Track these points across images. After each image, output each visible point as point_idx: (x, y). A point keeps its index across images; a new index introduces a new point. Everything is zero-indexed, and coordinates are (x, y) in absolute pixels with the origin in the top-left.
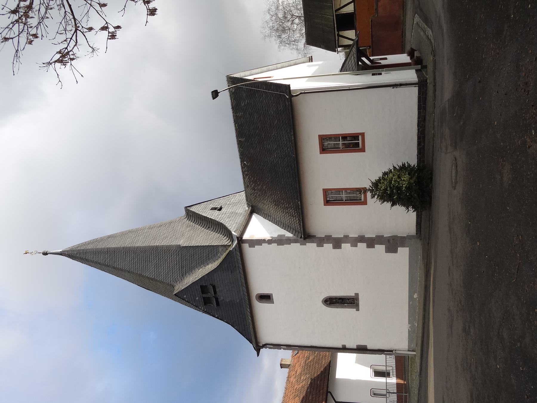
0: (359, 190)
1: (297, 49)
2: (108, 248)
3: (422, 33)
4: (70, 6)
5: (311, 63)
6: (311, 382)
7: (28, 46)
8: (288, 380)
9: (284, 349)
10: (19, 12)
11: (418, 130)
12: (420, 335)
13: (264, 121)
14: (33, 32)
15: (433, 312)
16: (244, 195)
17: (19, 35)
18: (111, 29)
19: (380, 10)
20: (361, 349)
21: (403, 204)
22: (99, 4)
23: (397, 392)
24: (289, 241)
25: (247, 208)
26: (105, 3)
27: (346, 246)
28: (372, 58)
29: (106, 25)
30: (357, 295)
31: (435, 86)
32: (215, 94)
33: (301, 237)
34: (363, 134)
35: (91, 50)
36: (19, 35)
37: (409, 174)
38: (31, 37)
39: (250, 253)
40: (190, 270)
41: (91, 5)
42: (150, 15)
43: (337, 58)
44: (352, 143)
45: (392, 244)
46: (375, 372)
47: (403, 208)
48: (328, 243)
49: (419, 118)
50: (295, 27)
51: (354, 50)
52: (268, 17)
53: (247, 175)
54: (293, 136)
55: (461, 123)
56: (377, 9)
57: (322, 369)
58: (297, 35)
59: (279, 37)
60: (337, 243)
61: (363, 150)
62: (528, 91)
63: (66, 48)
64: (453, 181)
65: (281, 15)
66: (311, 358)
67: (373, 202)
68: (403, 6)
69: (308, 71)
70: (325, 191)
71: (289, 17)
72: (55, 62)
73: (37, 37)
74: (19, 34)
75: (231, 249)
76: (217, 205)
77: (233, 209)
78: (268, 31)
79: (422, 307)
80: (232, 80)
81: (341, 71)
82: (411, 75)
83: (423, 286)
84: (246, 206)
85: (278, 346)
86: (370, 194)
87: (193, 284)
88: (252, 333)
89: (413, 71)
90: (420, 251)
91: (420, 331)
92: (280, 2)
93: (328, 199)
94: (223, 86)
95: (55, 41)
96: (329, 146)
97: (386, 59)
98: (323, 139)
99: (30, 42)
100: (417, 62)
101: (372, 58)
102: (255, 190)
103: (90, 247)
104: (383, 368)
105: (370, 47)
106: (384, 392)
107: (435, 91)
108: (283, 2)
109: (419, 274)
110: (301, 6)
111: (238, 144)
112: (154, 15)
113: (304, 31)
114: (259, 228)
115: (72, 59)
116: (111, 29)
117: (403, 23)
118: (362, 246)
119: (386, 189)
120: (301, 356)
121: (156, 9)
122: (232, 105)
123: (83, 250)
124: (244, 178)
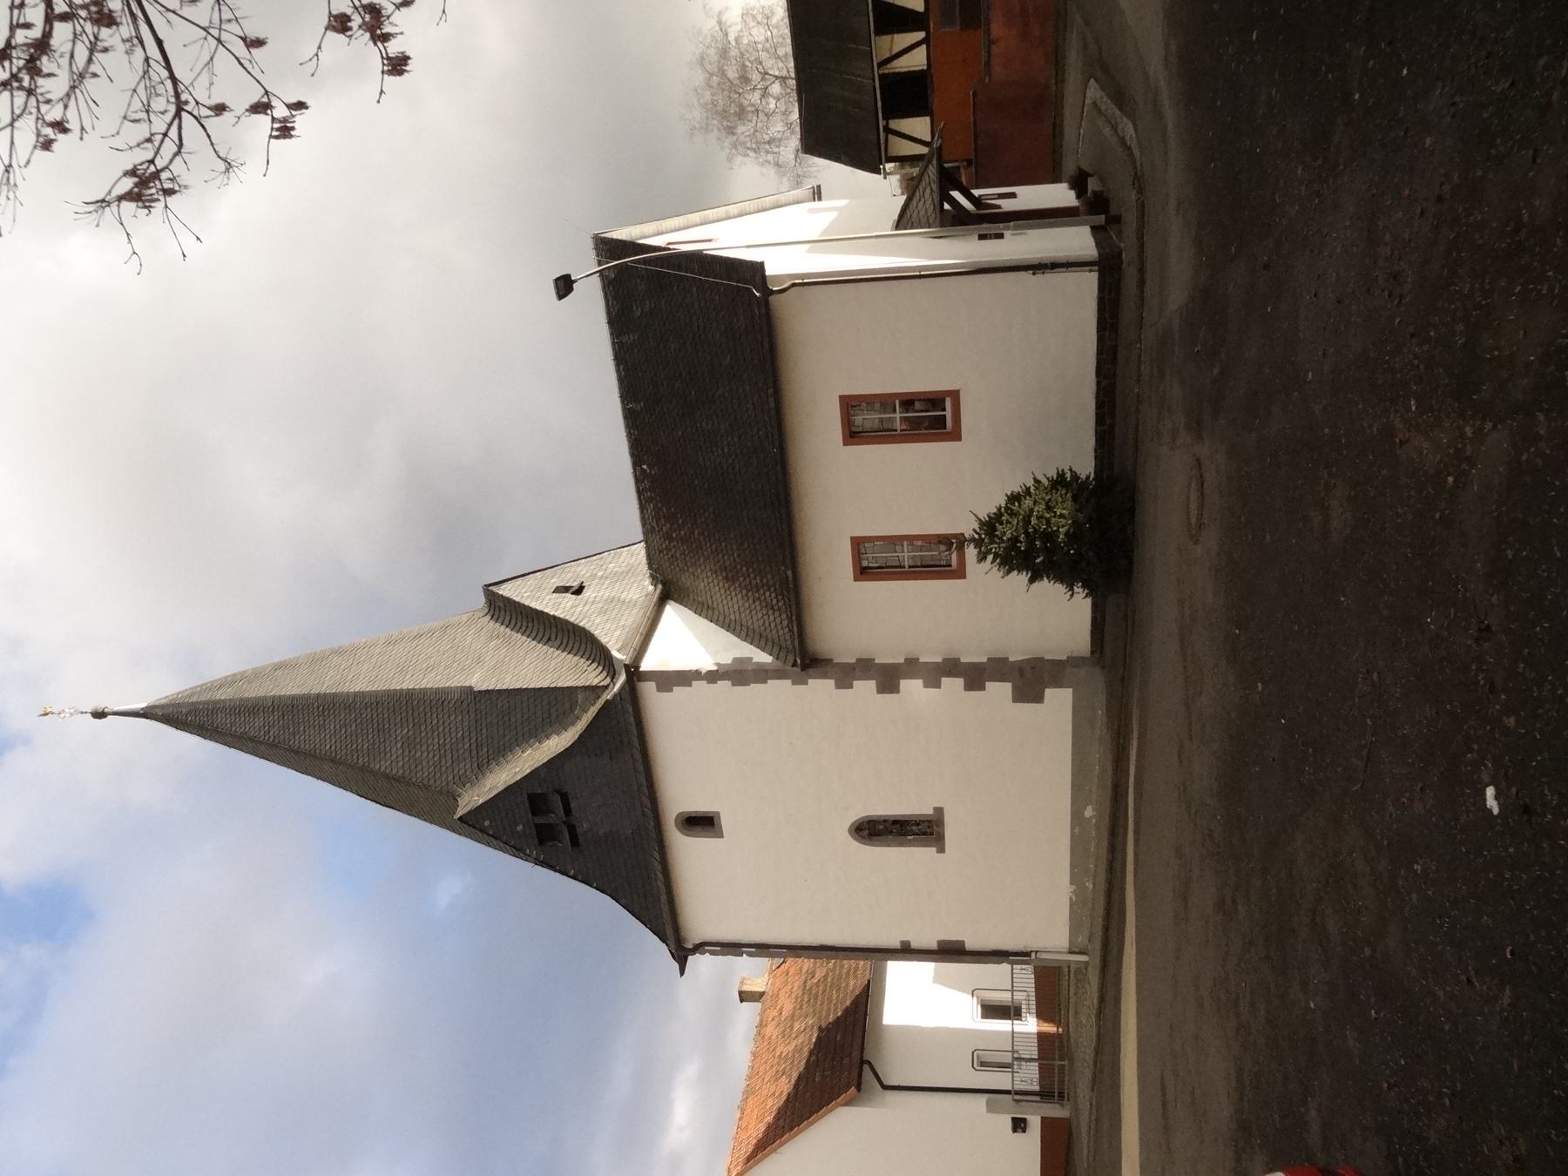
0: (946, 541)
1: (777, 165)
2: (273, 698)
3: (1107, 131)
4: (159, 43)
5: (817, 204)
6: (819, 1038)
7: (39, 153)
8: (759, 1033)
9: (750, 955)
10: (10, 58)
11: (1098, 383)
12: (1100, 911)
13: (697, 365)
14: (54, 114)
15: (1136, 854)
16: (643, 552)
17: (11, 125)
18: (280, 111)
19: (997, 68)
20: (950, 952)
21: (1060, 578)
22: (244, 39)
23: (1041, 1058)
24: (761, 675)
25: (651, 588)
26: (262, 36)
27: (912, 687)
28: (976, 192)
29: (265, 100)
30: (939, 811)
31: (1141, 270)
32: (564, 286)
33: (794, 665)
34: (955, 395)
35: (222, 166)
36: (11, 125)
37: (1075, 499)
38: (49, 131)
39: (660, 708)
40: (500, 751)
41: (219, 41)
42: (390, 73)
43: (883, 191)
44: (928, 416)
45: (1030, 679)
46: (983, 1007)
47: (1059, 589)
48: (865, 676)
49: (1100, 352)
50: (772, 106)
51: (932, 171)
52: (699, 78)
53: (650, 500)
54: (771, 400)
55: (1216, 371)
56: (988, 63)
57: (848, 1003)
58: (777, 128)
59: (731, 131)
60: (889, 678)
61: (956, 435)
62: (1401, 296)
63: (152, 162)
64: (1193, 521)
65: (732, 73)
66: (819, 974)
67: (982, 574)
68: (1057, 59)
69: (806, 224)
70: (858, 544)
71: (756, 77)
72: (120, 198)
73: (65, 131)
74: (14, 120)
75: (608, 695)
76: (569, 577)
77: (612, 588)
78: (697, 115)
79: (1105, 843)
80: (608, 248)
81: (897, 228)
82: (1078, 241)
83: (1109, 783)
84: (647, 582)
85: (733, 948)
86: (975, 552)
87: (510, 790)
88: (666, 916)
89: (1085, 231)
90: (1102, 698)
91: (1101, 901)
92: (732, 38)
93: (865, 563)
94: (584, 267)
95: (118, 142)
96: (868, 426)
97: (1013, 195)
98: (849, 405)
99: (47, 145)
100: (1095, 206)
101: (976, 192)
102: (671, 539)
103: (220, 695)
104: (1004, 997)
105: (969, 162)
106: (1007, 1058)
107: (1142, 283)
108: (737, 40)
109: (1099, 755)
110: (787, 49)
111: (625, 418)
112: (400, 73)
113: (795, 116)
114: (684, 641)
115: (169, 192)
116: (280, 111)
117: (1058, 102)
118: (953, 684)
119: (1015, 540)
120: (792, 970)
121: (408, 58)
122: (609, 313)
123: (207, 703)
124: (642, 508)
